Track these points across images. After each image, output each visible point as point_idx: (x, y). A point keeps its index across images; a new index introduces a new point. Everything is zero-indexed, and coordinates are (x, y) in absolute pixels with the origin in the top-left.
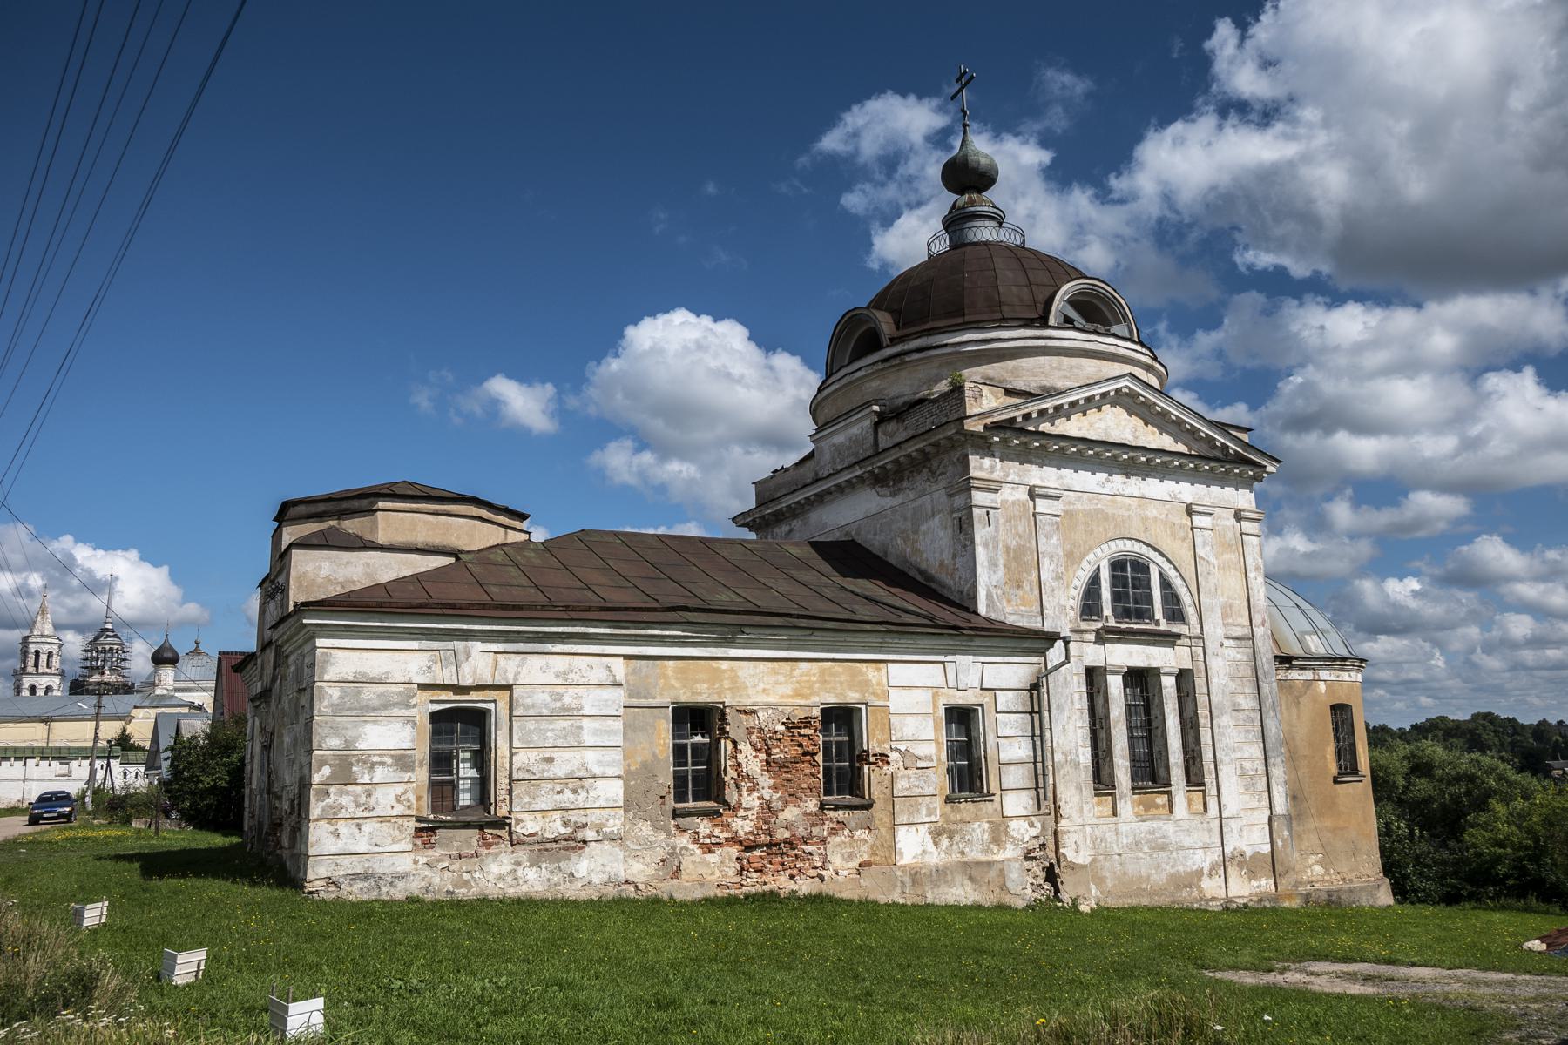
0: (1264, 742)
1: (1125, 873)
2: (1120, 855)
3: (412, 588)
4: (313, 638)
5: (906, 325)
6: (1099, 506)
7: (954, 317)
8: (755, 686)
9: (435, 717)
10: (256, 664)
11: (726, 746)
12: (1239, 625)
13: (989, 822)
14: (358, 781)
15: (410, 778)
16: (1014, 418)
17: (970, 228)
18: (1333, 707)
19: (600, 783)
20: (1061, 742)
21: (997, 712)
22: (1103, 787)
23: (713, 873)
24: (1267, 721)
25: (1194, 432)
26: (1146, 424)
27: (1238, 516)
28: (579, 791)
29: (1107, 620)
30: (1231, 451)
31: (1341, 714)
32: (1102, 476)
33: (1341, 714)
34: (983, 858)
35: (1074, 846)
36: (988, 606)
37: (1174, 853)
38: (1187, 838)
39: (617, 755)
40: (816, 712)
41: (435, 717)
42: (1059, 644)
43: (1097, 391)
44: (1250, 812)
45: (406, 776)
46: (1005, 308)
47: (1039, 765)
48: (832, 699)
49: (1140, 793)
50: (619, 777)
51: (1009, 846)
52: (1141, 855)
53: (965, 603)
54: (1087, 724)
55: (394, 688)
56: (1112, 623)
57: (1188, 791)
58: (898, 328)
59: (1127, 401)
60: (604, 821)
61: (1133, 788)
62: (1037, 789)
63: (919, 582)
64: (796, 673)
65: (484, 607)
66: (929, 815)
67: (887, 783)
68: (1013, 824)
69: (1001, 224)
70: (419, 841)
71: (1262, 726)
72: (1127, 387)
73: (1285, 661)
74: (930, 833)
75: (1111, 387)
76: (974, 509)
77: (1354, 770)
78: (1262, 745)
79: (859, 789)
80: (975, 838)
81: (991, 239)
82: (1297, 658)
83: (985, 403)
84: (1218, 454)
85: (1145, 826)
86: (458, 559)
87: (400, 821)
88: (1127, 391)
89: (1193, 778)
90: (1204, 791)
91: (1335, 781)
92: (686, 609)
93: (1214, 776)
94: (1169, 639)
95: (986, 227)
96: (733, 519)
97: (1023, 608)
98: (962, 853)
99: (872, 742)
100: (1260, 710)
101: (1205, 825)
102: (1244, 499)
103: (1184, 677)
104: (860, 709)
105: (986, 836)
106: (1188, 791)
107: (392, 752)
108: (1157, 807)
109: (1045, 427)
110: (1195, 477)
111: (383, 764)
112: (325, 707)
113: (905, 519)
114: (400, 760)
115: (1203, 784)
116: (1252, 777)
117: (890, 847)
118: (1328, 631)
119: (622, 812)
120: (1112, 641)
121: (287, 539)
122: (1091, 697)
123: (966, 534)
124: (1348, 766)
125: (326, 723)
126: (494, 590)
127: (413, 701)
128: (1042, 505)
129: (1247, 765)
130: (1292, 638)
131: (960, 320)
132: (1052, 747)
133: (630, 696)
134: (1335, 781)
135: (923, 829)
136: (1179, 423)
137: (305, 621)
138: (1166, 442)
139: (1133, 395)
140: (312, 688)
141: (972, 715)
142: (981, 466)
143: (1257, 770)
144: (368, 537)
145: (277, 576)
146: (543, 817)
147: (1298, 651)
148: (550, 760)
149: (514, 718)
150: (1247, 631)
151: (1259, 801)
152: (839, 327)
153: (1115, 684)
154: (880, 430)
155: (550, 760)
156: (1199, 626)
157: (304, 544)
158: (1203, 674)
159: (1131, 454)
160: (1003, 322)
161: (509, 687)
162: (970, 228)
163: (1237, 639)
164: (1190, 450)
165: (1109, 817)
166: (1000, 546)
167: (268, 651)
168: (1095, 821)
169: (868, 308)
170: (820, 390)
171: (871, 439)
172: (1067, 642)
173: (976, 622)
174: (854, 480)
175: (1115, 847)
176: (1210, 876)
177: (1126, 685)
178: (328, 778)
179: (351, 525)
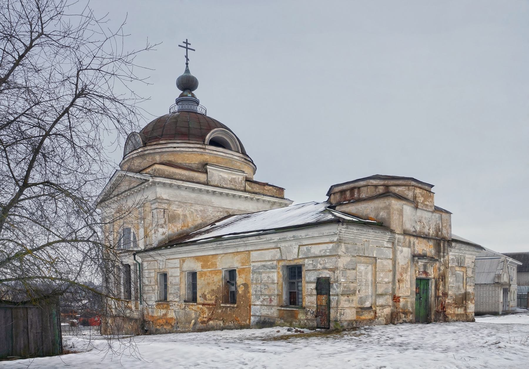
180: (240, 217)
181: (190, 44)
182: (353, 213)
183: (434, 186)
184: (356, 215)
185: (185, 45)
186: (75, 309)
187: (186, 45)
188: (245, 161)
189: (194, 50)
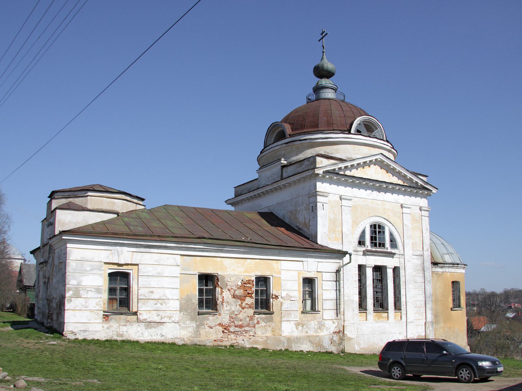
0: (425, 295)
3: (102, 226)
4: (66, 243)
5: (296, 130)
7: (314, 128)
8: (230, 268)
9: (110, 275)
10: (40, 252)
11: (218, 290)
12: (419, 250)
13: (317, 321)
14: (82, 297)
15: (101, 296)
16: (335, 169)
17: (323, 92)
18: (453, 282)
19: (171, 301)
21: (323, 281)
22: (364, 310)
23: (212, 336)
24: (426, 287)
25: (405, 176)
26: (387, 172)
27: (421, 209)
28: (163, 304)
29: (367, 247)
30: (419, 184)
31: (456, 285)
32: (369, 192)
33: (456, 285)
34: (315, 334)
36: (321, 240)
39: (177, 292)
40: (253, 278)
41: (110, 275)
42: (348, 256)
43: (368, 160)
44: (418, 320)
45: (99, 296)
46: (334, 126)
47: (338, 301)
48: (260, 274)
49: (376, 312)
50: (178, 299)
51: (325, 330)
52: (375, 335)
53: (312, 238)
54: (357, 286)
55: (95, 263)
56: (369, 248)
57: (395, 312)
58: (293, 131)
59: (377, 163)
60: (172, 315)
61: (374, 310)
62: (337, 310)
63: (296, 230)
64: (246, 264)
65: (128, 235)
66: (295, 318)
67: (279, 305)
69: (336, 91)
70: (104, 319)
71: (425, 289)
72: (380, 158)
73: (435, 264)
74: (295, 325)
75: (373, 158)
76: (318, 203)
77: (459, 306)
78: (424, 296)
79: (268, 308)
80: (312, 327)
81: (331, 97)
82: (440, 264)
83: (322, 164)
84: (414, 185)
86: (118, 215)
87: (97, 312)
88: (380, 160)
89: (397, 307)
90: (401, 312)
91: (452, 310)
92: (204, 238)
93: (405, 307)
94: (391, 255)
95: (330, 92)
96: (225, 201)
98: (307, 332)
99: (273, 291)
100: (424, 283)
102: (423, 202)
103: (396, 270)
104: (270, 278)
105: (316, 326)
106: (395, 312)
107: (95, 287)
108: (383, 317)
109: (348, 173)
110: (405, 193)
111: (91, 291)
112: (70, 269)
113: (292, 205)
114: (97, 290)
115: (401, 310)
118: (453, 254)
119: (178, 312)
120: (369, 255)
121: (54, 206)
122: (360, 275)
123: (314, 213)
124: (457, 304)
125: (71, 275)
126: (132, 228)
127: (102, 268)
128: (344, 202)
129: (418, 303)
130: (439, 256)
131: (317, 129)
132: (344, 294)
133: (183, 270)
134: (452, 310)
135: (292, 323)
136: (399, 173)
137: (64, 238)
138: (395, 180)
139: (382, 162)
140: (66, 262)
141: (313, 281)
142: (321, 186)
144: (84, 206)
145: (49, 219)
146: (150, 313)
147: (441, 261)
148: (152, 292)
149: (139, 276)
150: (421, 253)
152: (270, 129)
153: (369, 273)
154: (284, 170)
155: (152, 292)
156: (403, 250)
157: (61, 208)
158: (404, 269)
159: (380, 184)
160: (333, 130)
161: (137, 265)
162: (323, 92)
163: (418, 256)
164: (404, 183)
165: (364, 321)
166: (327, 217)
167: (46, 247)
169: (281, 122)
170: (261, 153)
171: (280, 173)
172: (350, 255)
173: (316, 246)
174: (273, 189)
177: (373, 271)
178: (71, 295)
179: (78, 201)
188: (287, 145)
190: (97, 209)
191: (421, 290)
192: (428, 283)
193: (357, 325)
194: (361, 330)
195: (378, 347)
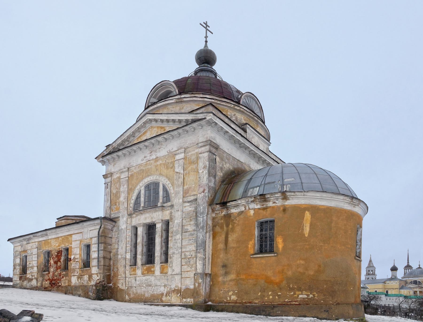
1: (137, 293)
2: (135, 287)
6: (141, 168)
20: (121, 251)
35: (121, 284)
37: (153, 287)
38: (159, 282)
66: (77, 273)
68: (93, 276)
85: (144, 278)
97: (116, 211)
101: (166, 277)
105: (88, 279)
116: (189, 258)
117: (70, 281)
135: (76, 277)
143: (192, 255)
151: (191, 268)
168: (129, 276)
175: (134, 285)
176: (166, 296)
180: (137, 200)
181: (209, 27)
182: (95, 221)
183: (57, 219)
184: (315, 192)
185: (205, 26)
186: (120, 282)
187: (206, 26)
189: (212, 33)
190: (59, 228)
191: (193, 239)
192: (201, 230)
193: (128, 278)
194: (130, 283)
195: (144, 298)
